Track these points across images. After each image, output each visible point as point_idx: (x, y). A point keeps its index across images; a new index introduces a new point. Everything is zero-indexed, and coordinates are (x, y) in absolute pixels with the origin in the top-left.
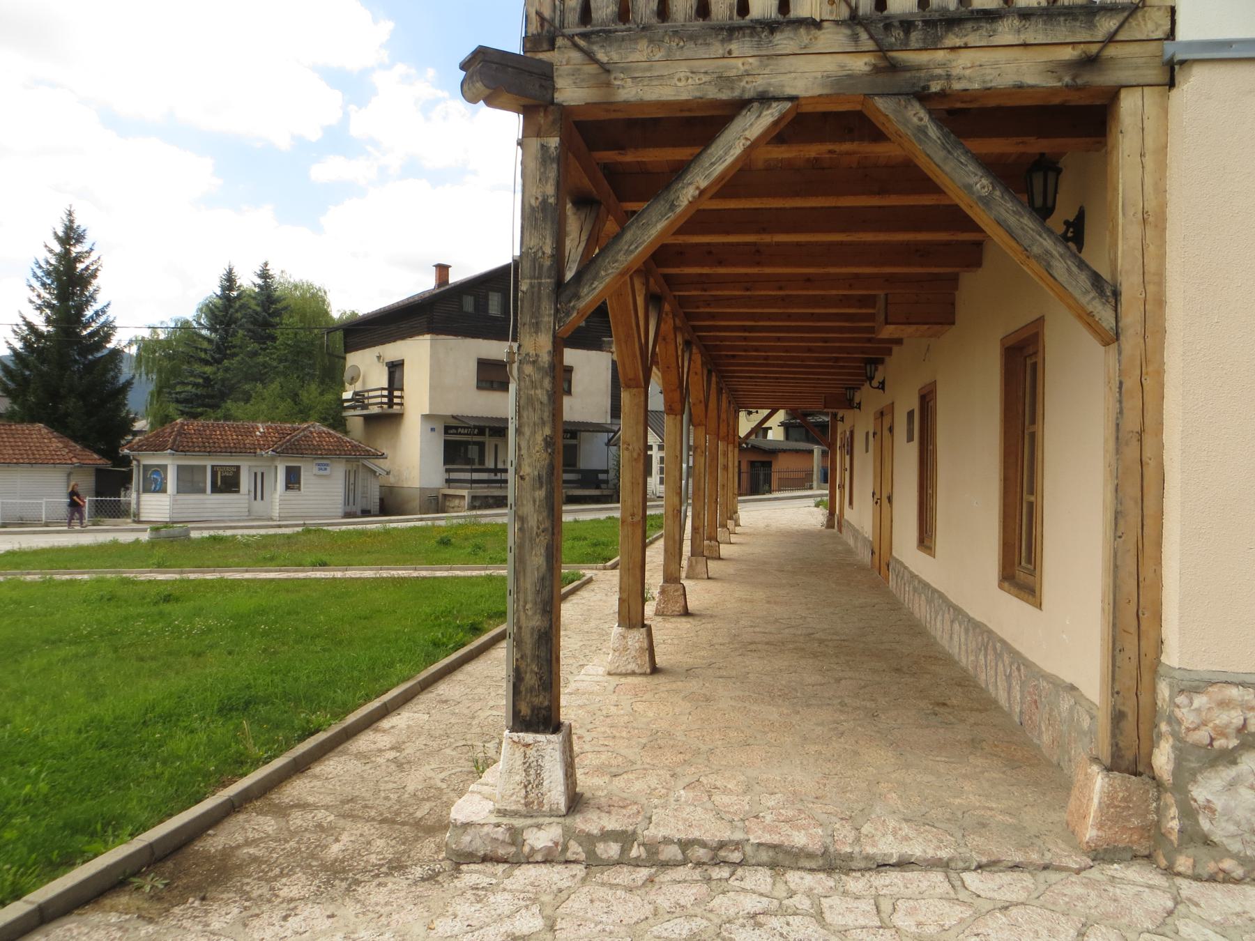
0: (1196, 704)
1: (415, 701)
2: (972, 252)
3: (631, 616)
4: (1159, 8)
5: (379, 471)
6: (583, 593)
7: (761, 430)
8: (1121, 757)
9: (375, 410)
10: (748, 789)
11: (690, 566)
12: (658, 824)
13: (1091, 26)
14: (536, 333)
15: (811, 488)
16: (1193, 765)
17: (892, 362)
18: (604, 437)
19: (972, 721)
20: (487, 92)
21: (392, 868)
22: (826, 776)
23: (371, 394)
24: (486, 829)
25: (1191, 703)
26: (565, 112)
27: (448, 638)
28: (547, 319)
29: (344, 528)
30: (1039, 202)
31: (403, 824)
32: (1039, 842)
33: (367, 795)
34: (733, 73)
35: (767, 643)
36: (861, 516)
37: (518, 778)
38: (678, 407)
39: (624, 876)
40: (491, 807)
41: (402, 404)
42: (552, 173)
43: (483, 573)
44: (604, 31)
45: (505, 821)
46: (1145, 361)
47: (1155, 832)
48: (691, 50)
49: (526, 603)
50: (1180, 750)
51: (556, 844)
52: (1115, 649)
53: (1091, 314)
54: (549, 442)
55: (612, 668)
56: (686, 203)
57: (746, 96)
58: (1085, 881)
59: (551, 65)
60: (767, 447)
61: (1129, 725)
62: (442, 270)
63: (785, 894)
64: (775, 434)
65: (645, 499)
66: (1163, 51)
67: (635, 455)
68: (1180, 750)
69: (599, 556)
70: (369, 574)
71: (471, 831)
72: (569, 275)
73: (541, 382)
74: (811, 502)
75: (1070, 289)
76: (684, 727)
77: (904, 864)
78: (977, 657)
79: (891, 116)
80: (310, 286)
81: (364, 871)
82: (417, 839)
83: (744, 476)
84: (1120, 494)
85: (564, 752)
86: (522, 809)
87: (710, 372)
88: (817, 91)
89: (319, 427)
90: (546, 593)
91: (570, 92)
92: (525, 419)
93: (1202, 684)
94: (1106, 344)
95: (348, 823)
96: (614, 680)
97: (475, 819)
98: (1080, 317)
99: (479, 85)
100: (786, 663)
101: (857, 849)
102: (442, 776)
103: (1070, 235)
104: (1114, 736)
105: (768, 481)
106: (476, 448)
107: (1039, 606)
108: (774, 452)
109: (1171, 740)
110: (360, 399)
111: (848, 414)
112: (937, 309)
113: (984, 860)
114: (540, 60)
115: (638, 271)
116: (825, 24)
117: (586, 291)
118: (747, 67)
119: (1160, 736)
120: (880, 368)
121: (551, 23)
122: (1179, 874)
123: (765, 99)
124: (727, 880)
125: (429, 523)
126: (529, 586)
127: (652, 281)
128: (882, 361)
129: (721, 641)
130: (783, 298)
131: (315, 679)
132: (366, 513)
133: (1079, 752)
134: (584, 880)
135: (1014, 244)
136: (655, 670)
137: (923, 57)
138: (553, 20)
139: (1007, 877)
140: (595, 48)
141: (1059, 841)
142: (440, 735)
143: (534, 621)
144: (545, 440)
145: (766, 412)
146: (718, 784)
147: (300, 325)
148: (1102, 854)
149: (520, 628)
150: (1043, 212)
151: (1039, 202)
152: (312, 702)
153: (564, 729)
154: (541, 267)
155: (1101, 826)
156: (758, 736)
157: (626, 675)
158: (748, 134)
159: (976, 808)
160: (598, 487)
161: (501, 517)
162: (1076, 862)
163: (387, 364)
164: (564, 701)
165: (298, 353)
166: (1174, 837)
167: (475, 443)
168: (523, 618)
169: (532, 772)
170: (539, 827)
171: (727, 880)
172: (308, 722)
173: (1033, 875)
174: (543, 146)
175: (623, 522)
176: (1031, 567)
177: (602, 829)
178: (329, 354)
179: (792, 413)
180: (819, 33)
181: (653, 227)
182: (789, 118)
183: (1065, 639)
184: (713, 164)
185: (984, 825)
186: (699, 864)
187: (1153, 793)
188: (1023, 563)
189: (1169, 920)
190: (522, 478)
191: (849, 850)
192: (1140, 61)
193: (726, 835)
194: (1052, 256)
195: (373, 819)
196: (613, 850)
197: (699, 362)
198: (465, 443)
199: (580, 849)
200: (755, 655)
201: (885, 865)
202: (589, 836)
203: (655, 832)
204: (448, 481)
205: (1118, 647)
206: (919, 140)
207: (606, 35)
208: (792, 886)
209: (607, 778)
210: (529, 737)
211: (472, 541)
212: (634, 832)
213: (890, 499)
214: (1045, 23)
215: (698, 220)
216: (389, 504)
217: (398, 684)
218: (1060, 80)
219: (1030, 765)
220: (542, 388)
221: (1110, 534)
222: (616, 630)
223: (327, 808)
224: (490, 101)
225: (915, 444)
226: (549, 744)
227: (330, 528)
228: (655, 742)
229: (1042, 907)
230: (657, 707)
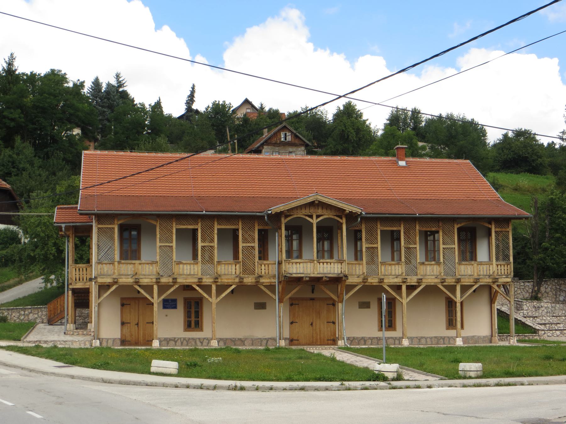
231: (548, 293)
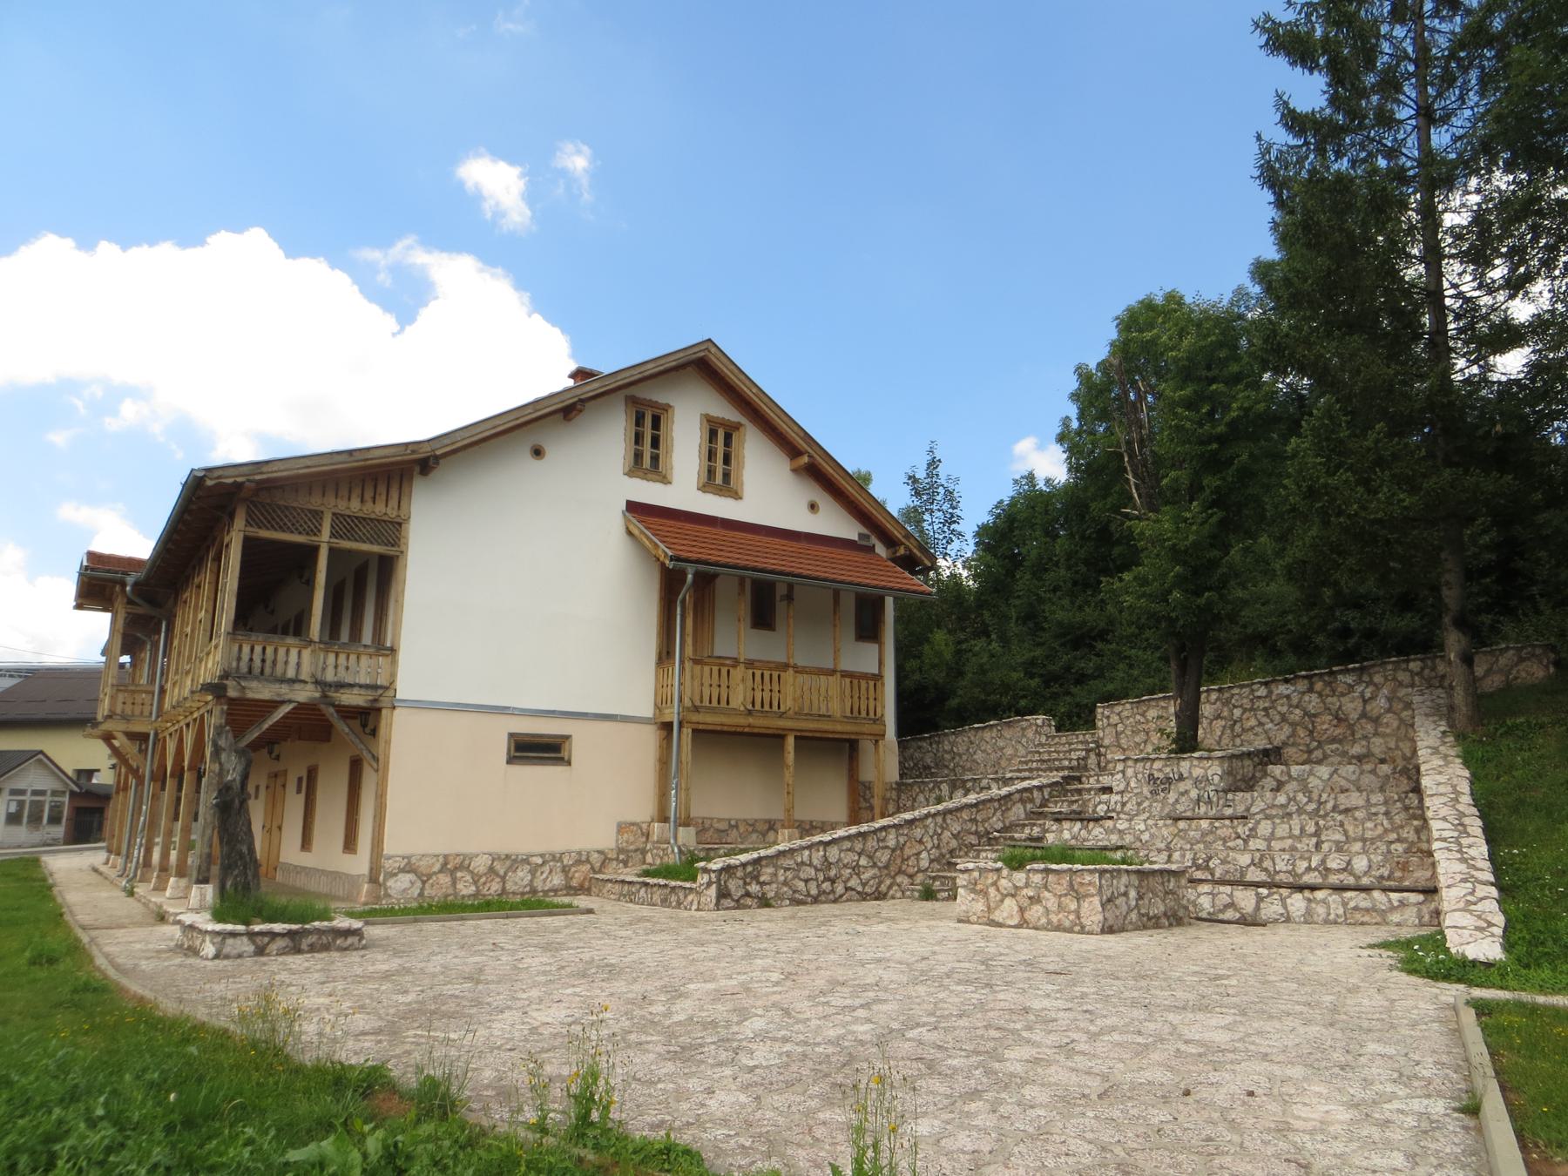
91: (232, 693)
123: (290, 701)
207: (245, 678)
213: (280, 828)
225: (303, 795)
231: (1376, 721)
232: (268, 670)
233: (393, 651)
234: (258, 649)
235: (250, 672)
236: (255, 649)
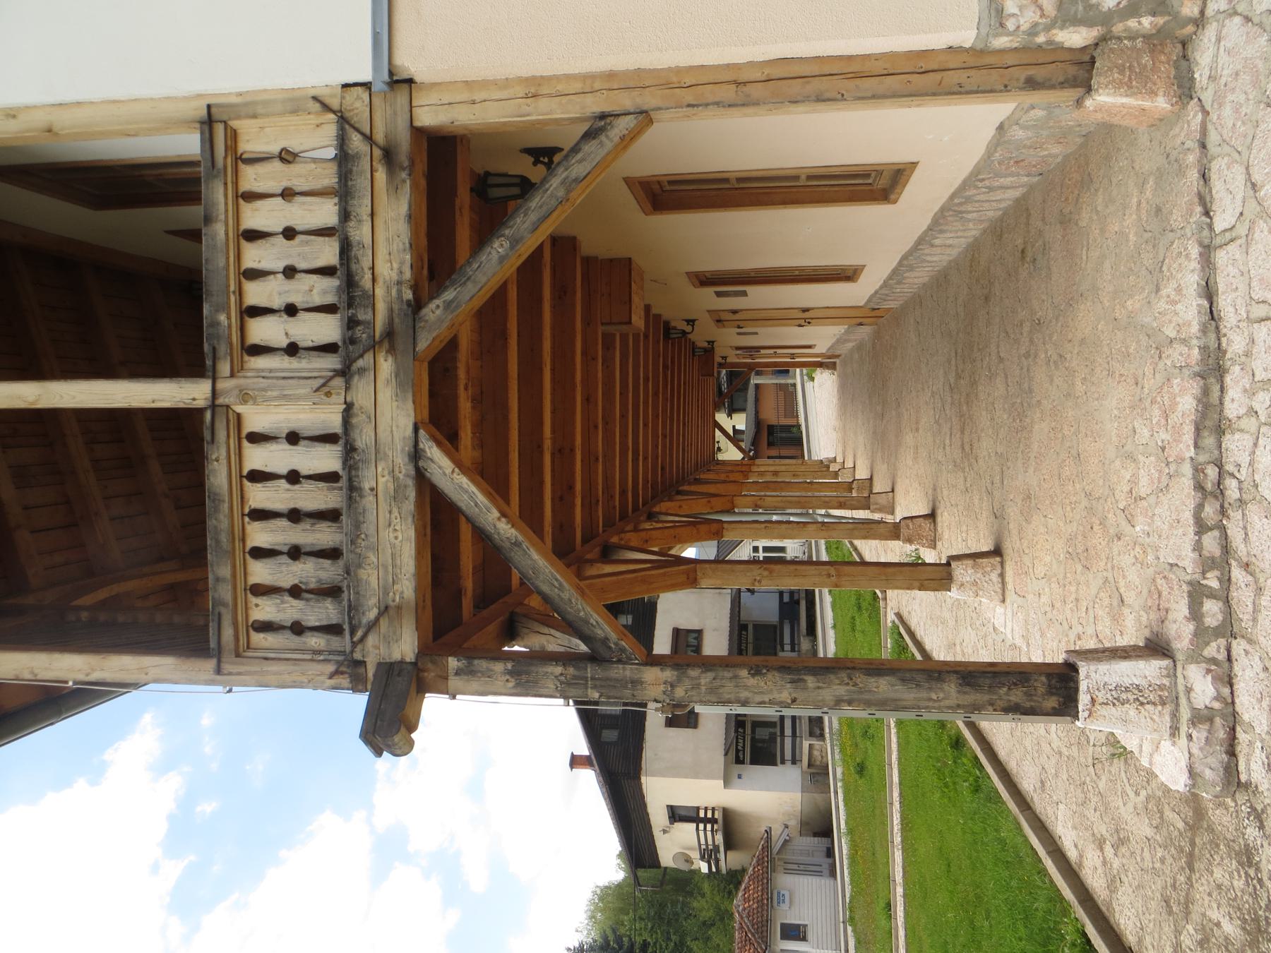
0: (1016, 11)
1: (1043, 818)
2: (563, 245)
3: (938, 577)
4: (343, 98)
5: (785, 836)
6: (913, 624)
7: (736, 437)
8: (1075, 78)
9: (719, 838)
10: (1131, 457)
11: (880, 510)
12: (1178, 557)
13: (357, 156)
14: (642, 683)
15: (794, 385)
16: (1081, 8)
17: (667, 314)
18: (745, 596)
19: (1039, 224)
20: (403, 730)
21: (1250, 865)
22: (1111, 374)
23: (703, 841)
24: (1195, 751)
25: (1013, 15)
26: (425, 651)
27: (970, 786)
28: (627, 672)
29: (847, 879)
30: (516, 191)
31: (1193, 844)
32: (1174, 154)
33: (1160, 884)
34: (391, 486)
35: (962, 432)
36: (822, 338)
37: (1132, 713)
38: (714, 527)
39: (1242, 596)
40: (1168, 743)
41: (713, 809)
42: (481, 664)
43: (894, 731)
44: (349, 612)
45: (1184, 729)
46: (668, 85)
47: (1154, 41)
48: (368, 528)
49: (930, 699)
50: (1064, 22)
51: (1208, 671)
52: (960, 91)
53: (622, 138)
54: (756, 671)
55: (998, 597)
56: (513, 531)
57: (413, 473)
58: (1216, 106)
59: (379, 665)
60: (753, 430)
61: (1039, 73)
62: (575, 761)
63: (1253, 419)
64: (740, 422)
65: (810, 562)
66: (380, 92)
67: (766, 573)
68: (1064, 22)
69: (873, 607)
70: (898, 856)
71: (1198, 768)
72: (583, 648)
73: (692, 678)
74: (809, 385)
75: (598, 158)
76: (1061, 524)
77: (1209, 292)
78: (969, 220)
79: (434, 334)
80: (591, 901)
81: (1255, 895)
82: (1211, 829)
83: (784, 452)
84: (799, 98)
85: (1099, 660)
86: (1168, 709)
87: (679, 493)
88: (410, 405)
89: (738, 900)
90: (919, 677)
91: (405, 646)
92: (732, 697)
93: (994, 6)
94: (651, 121)
95: (1196, 909)
96: (1010, 596)
97: (1183, 763)
98: (625, 148)
99: (396, 738)
100: (984, 413)
101: (1195, 342)
102: (1132, 794)
103: (546, 160)
104: (1052, 87)
105: (787, 428)
106: (758, 730)
107: (914, 165)
108: (758, 423)
109: (1054, 31)
110: (709, 854)
111: (719, 352)
112: (616, 274)
113: (1199, 209)
114: (375, 676)
115: (579, 575)
116: (349, 399)
117: (599, 632)
118: (386, 473)
119: (1050, 42)
120: (673, 324)
121: (340, 664)
122: (1202, 12)
123: (416, 455)
124: (1240, 482)
125: (839, 784)
126: (912, 695)
127: (588, 556)
128: (667, 324)
129: (962, 479)
130: (606, 423)
131: (1022, 932)
132: (830, 853)
133: (1069, 117)
134: (1250, 641)
135: (555, 214)
136: (997, 552)
137: (381, 307)
138: (337, 662)
139: (1217, 186)
140: (364, 621)
141: (1172, 133)
142: (1083, 792)
143: (951, 690)
144: (753, 675)
145: (718, 433)
146: (1126, 489)
147: (631, 914)
148: (1185, 89)
149: (959, 706)
150: (526, 187)
151: (516, 191)
152: (1049, 937)
153: (1072, 660)
154: (575, 677)
155: (1153, 93)
156: (1068, 444)
157: (1003, 583)
158: (448, 471)
159: (1140, 219)
160: (798, 602)
161: (832, 722)
162: (1194, 116)
163: (672, 823)
164: (1037, 658)
165: (661, 918)
166: (1160, 21)
167: (753, 732)
168: (947, 703)
169: (1124, 696)
170: (1189, 690)
171: (1240, 482)
172: (1074, 945)
173: (1213, 158)
174: (457, 674)
175: (837, 586)
176: (873, 174)
177: (1188, 619)
178: (662, 884)
179: (717, 407)
180: (356, 406)
181: (536, 563)
182: (433, 430)
183: (947, 141)
184: (476, 505)
185: (1158, 210)
186: (1223, 512)
187: (1113, 44)
188: (870, 181)
189: (1256, 20)
190: (794, 701)
191: (1196, 351)
192: (389, 112)
193: (1187, 482)
194: (567, 178)
195: (1189, 878)
196: (1212, 609)
197: (669, 504)
198: (754, 745)
199: (1214, 644)
200: (976, 445)
201: (1211, 312)
202: (1196, 634)
203: (1188, 560)
204: (794, 762)
205: (957, 89)
206: (457, 307)
207: (353, 609)
208: (1242, 411)
209: (1126, 611)
210: (1083, 700)
211: (859, 740)
212: (1190, 583)
213: (805, 310)
214: (353, 198)
215: (530, 518)
216: (821, 827)
217: (1025, 836)
218: (404, 181)
219: (1087, 164)
220: (699, 678)
221: (841, 105)
222: (954, 593)
223: (1178, 932)
224: (412, 727)
225: (750, 289)
226: (1091, 677)
227: (848, 895)
228: (1080, 555)
229: (1250, 148)
230: (1040, 549)
232: (324, 535)
233: (210, 121)
234: (260, 572)
235: (331, 592)
236: (261, 570)
